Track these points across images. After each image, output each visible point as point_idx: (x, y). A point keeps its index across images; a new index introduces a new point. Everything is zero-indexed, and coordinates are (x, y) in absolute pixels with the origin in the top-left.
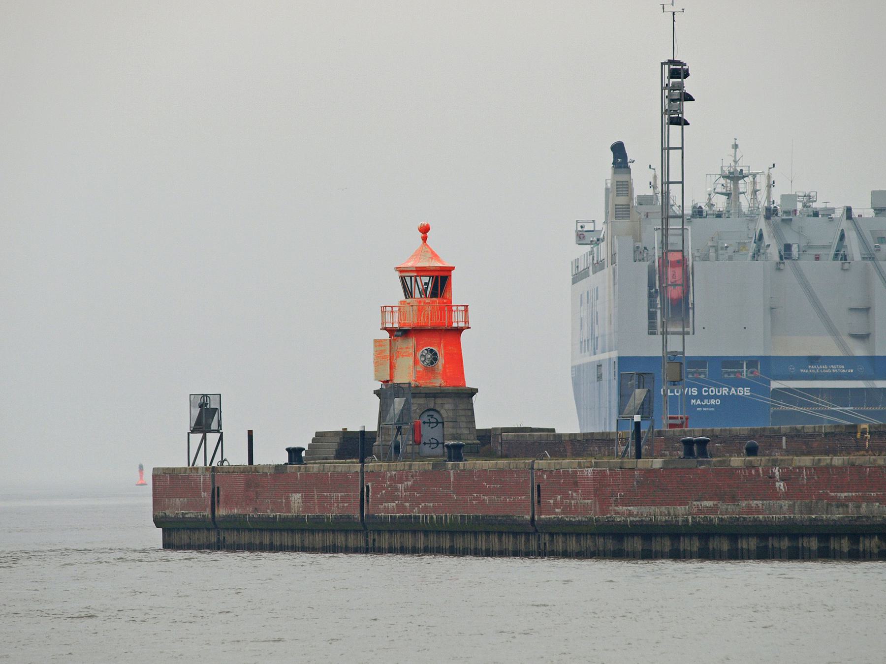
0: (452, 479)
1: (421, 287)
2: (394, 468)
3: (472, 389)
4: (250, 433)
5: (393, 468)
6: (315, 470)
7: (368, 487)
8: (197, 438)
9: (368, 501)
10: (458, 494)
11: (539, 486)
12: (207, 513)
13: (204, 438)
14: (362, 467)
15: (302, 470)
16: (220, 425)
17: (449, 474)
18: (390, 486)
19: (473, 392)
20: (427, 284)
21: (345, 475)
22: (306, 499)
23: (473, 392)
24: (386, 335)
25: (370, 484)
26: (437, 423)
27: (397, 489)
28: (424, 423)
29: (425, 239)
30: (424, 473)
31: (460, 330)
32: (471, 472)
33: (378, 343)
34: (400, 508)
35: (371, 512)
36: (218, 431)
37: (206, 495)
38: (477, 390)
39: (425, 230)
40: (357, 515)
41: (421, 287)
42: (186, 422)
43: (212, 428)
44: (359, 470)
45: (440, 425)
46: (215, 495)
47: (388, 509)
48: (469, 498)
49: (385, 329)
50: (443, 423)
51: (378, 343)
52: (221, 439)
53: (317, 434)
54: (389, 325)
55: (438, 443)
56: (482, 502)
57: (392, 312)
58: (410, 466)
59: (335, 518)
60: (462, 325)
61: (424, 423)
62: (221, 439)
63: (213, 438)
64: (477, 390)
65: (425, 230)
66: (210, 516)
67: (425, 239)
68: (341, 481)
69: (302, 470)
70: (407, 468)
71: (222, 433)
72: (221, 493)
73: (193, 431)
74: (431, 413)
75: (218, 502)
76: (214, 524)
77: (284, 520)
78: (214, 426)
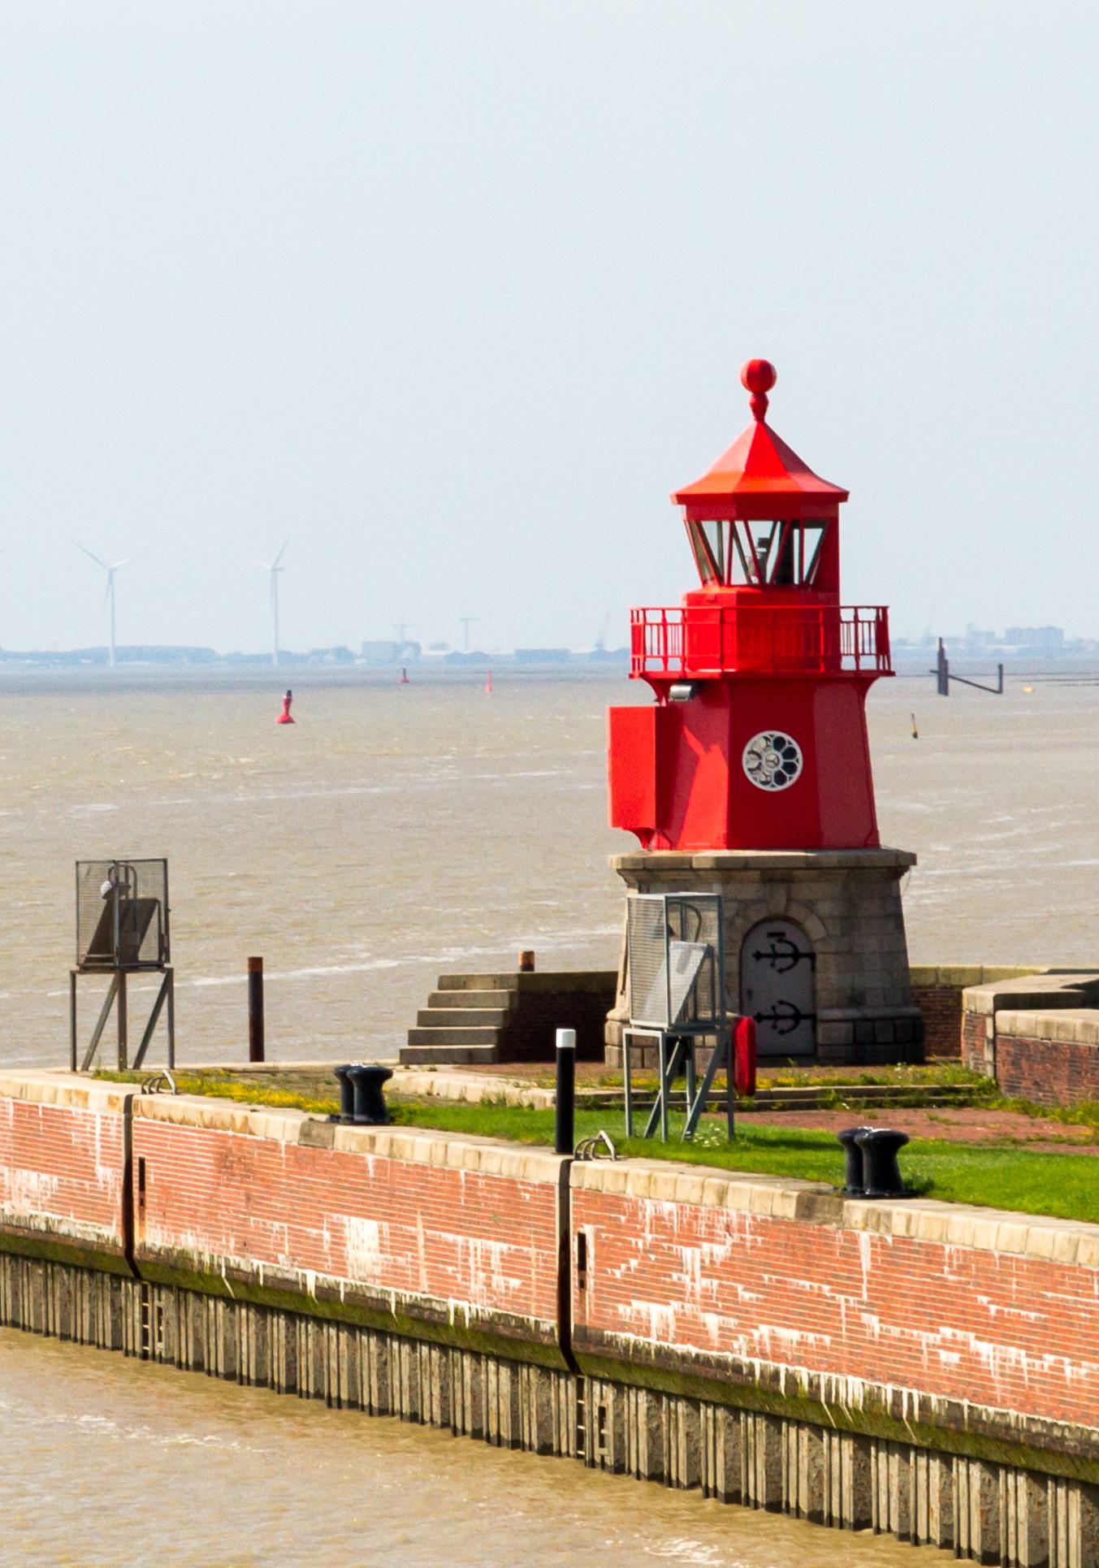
0: (866, 1263)
1: (748, 553)
2: (668, 1191)
3: (898, 854)
4: (256, 965)
5: (665, 1190)
6: (420, 1157)
7: (582, 1238)
8: (98, 986)
9: (582, 1284)
10: (886, 1316)
11: (142, 1162)
12: (112, 1232)
13: (120, 988)
14: (566, 1168)
15: (382, 1149)
16: (164, 949)
17: (854, 1240)
18: (655, 1248)
19: (901, 863)
20: (766, 543)
21: (511, 1186)
22: (397, 1243)
23: (901, 863)
24: (644, 697)
25: (588, 1230)
26: (796, 956)
27: (679, 1265)
28: (758, 956)
29: (760, 407)
30: (768, 1226)
31: (862, 681)
32: (932, 1254)
33: (621, 719)
34: (689, 1329)
35: (589, 1321)
36: (158, 966)
37: (109, 1177)
38: (912, 859)
39: (760, 378)
40: (550, 1323)
41: (748, 553)
42: (67, 946)
43: (142, 956)
44: (554, 1178)
45: (805, 962)
46: (133, 1178)
47: (649, 1322)
48: (927, 1338)
49: (645, 676)
50: (812, 956)
51: (621, 719)
52: (167, 988)
53: (446, 982)
54: (654, 665)
55: (797, 1017)
56: (971, 1361)
57: (664, 623)
58: (722, 1195)
59: (476, 1318)
60: (869, 663)
61: (758, 956)
62: (167, 988)
63: (143, 987)
64: (912, 859)
65: (760, 378)
66: (120, 1242)
67: (760, 407)
68: (496, 1209)
69: (382, 1149)
70: (710, 1198)
71: (169, 974)
72: (150, 1178)
73: (88, 966)
74: (777, 927)
75: (142, 1202)
76: (129, 1267)
77: (327, 1294)
78: (148, 951)
